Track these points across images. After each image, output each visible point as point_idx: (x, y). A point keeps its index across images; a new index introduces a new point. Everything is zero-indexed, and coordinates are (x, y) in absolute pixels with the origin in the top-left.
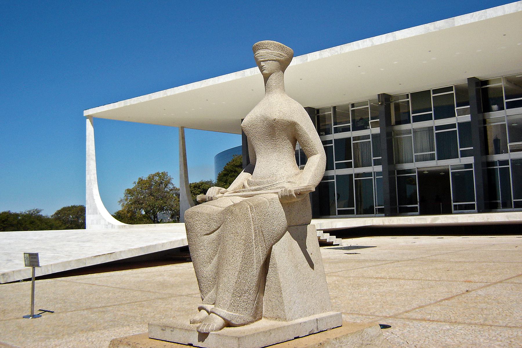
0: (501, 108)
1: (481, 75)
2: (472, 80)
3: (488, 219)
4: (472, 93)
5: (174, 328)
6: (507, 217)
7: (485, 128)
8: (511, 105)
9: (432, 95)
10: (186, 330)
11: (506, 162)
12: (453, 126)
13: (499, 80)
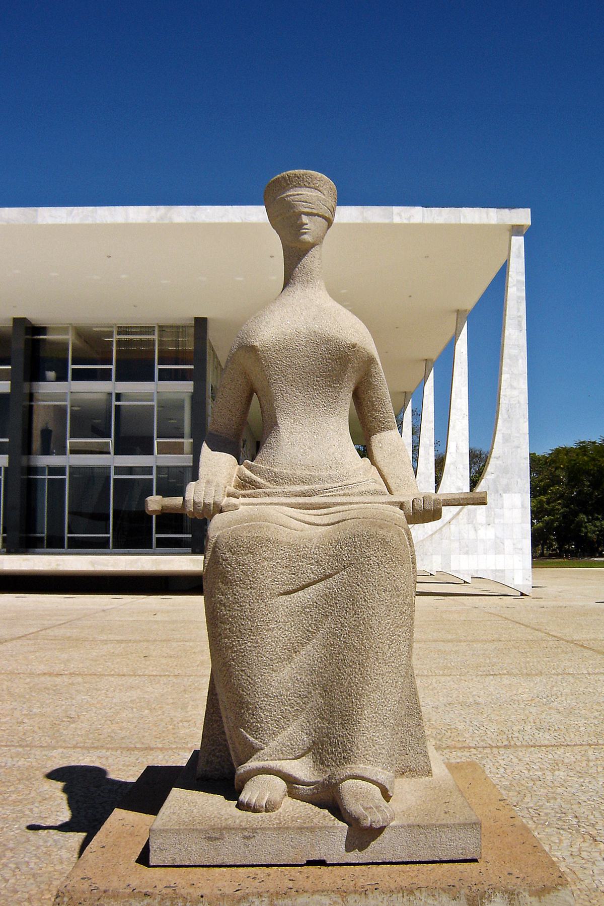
0: (62, 377)
1: (36, 315)
2: (19, 322)
3: (58, 565)
4: (19, 345)
5: (254, 830)
6: (93, 563)
7: (31, 408)
8: (79, 376)
10: (301, 828)
11: (60, 470)
13: (64, 330)
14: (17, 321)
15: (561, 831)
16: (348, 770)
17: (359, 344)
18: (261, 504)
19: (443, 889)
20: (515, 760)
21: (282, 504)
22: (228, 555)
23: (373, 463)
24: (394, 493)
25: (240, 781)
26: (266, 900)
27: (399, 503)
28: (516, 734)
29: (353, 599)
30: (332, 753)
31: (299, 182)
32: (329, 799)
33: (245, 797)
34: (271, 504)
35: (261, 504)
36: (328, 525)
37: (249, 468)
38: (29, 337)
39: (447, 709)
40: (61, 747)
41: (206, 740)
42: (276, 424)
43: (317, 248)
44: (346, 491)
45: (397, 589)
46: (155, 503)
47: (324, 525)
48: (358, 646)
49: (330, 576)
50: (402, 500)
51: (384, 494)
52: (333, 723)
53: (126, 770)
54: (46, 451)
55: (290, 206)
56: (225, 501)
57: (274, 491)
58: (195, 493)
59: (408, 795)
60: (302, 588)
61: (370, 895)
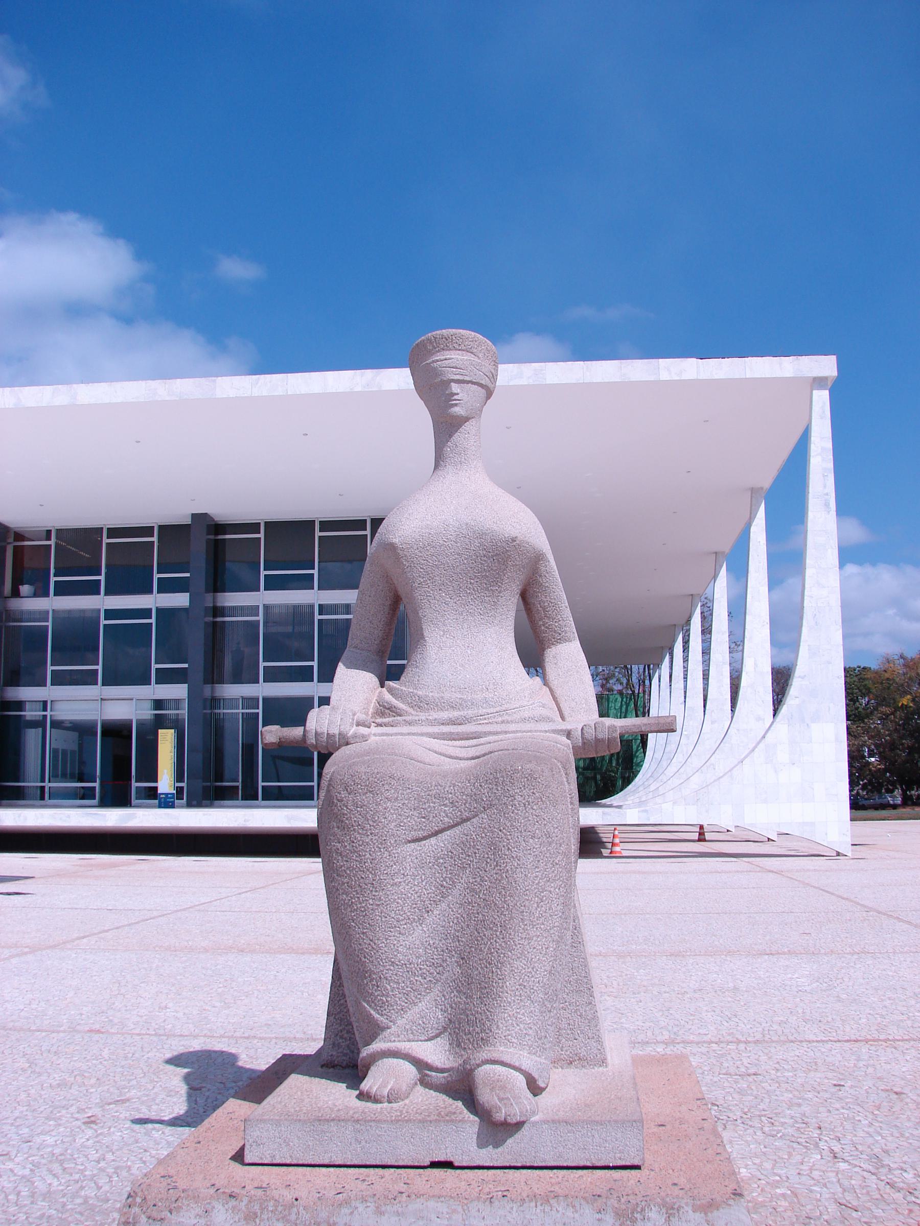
4: (199, 546)
9: (318, 534)
12: (146, 613)
14: (194, 516)
15: (795, 1145)
16: (484, 1055)
17: (520, 537)
18: (396, 734)
19: (584, 1198)
20: (764, 1058)
21: (422, 734)
22: (344, 794)
23: (546, 683)
24: (567, 719)
25: (364, 1066)
26: (372, 1205)
27: (565, 731)
28: (775, 1027)
29: (494, 847)
30: (470, 1033)
31: (447, 344)
32: (462, 1088)
33: (365, 1085)
34: (409, 734)
35: (396, 734)
36: (473, 758)
37: (391, 691)
38: (212, 537)
39: (697, 995)
40: (205, 1036)
41: (332, 1018)
42: (422, 636)
43: (472, 422)
44: (506, 718)
45: (548, 835)
46: (271, 734)
47: (468, 759)
48: (499, 903)
49: (468, 819)
50: (569, 727)
51: (549, 720)
52: (471, 997)
53: (259, 1059)
54: (238, 679)
55: (435, 373)
56: (352, 731)
57: (417, 718)
58: (319, 722)
59: (566, 1088)
60: (436, 833)
61: (496, 1203)
